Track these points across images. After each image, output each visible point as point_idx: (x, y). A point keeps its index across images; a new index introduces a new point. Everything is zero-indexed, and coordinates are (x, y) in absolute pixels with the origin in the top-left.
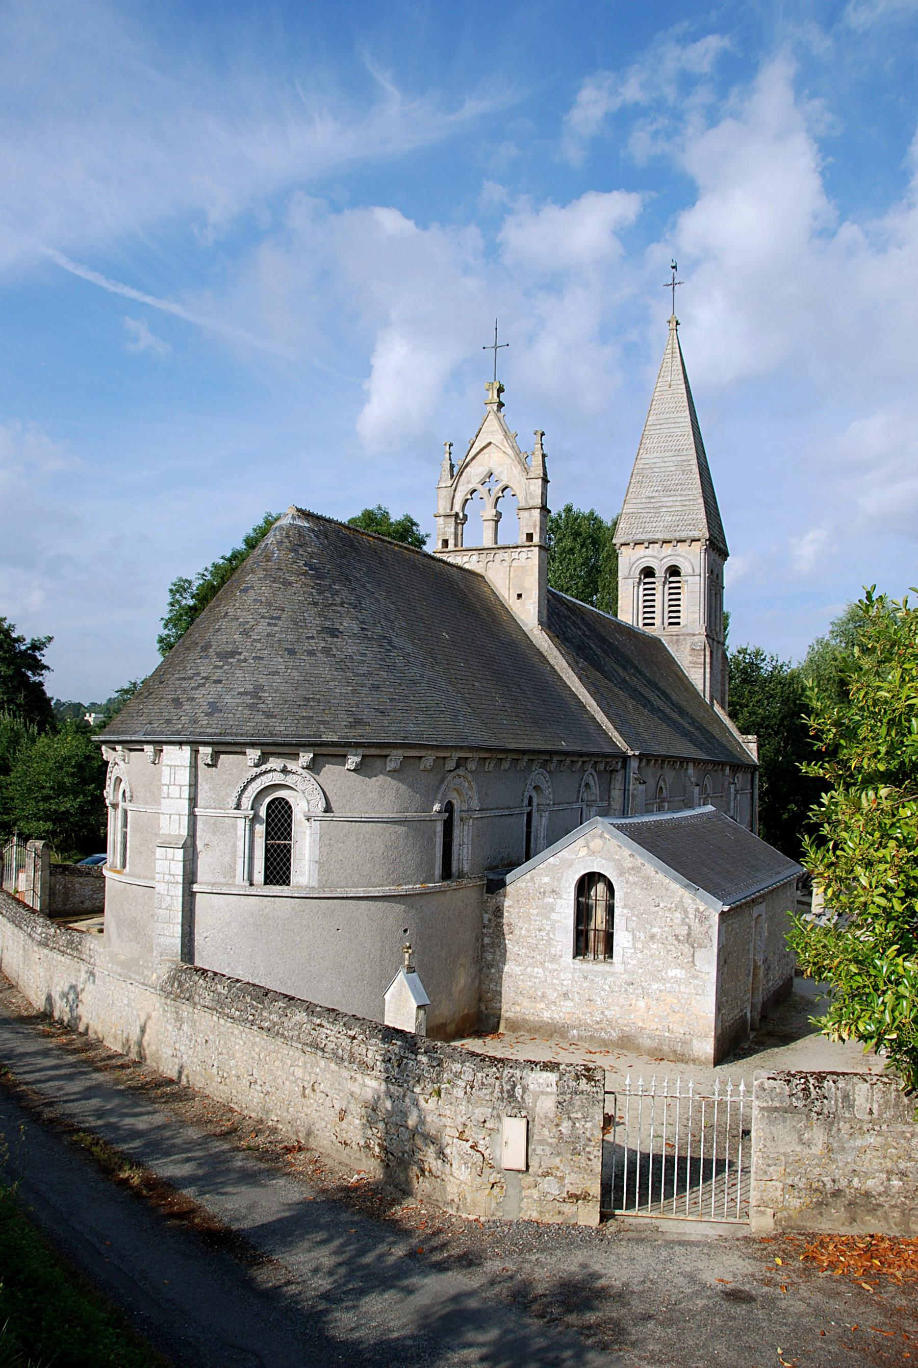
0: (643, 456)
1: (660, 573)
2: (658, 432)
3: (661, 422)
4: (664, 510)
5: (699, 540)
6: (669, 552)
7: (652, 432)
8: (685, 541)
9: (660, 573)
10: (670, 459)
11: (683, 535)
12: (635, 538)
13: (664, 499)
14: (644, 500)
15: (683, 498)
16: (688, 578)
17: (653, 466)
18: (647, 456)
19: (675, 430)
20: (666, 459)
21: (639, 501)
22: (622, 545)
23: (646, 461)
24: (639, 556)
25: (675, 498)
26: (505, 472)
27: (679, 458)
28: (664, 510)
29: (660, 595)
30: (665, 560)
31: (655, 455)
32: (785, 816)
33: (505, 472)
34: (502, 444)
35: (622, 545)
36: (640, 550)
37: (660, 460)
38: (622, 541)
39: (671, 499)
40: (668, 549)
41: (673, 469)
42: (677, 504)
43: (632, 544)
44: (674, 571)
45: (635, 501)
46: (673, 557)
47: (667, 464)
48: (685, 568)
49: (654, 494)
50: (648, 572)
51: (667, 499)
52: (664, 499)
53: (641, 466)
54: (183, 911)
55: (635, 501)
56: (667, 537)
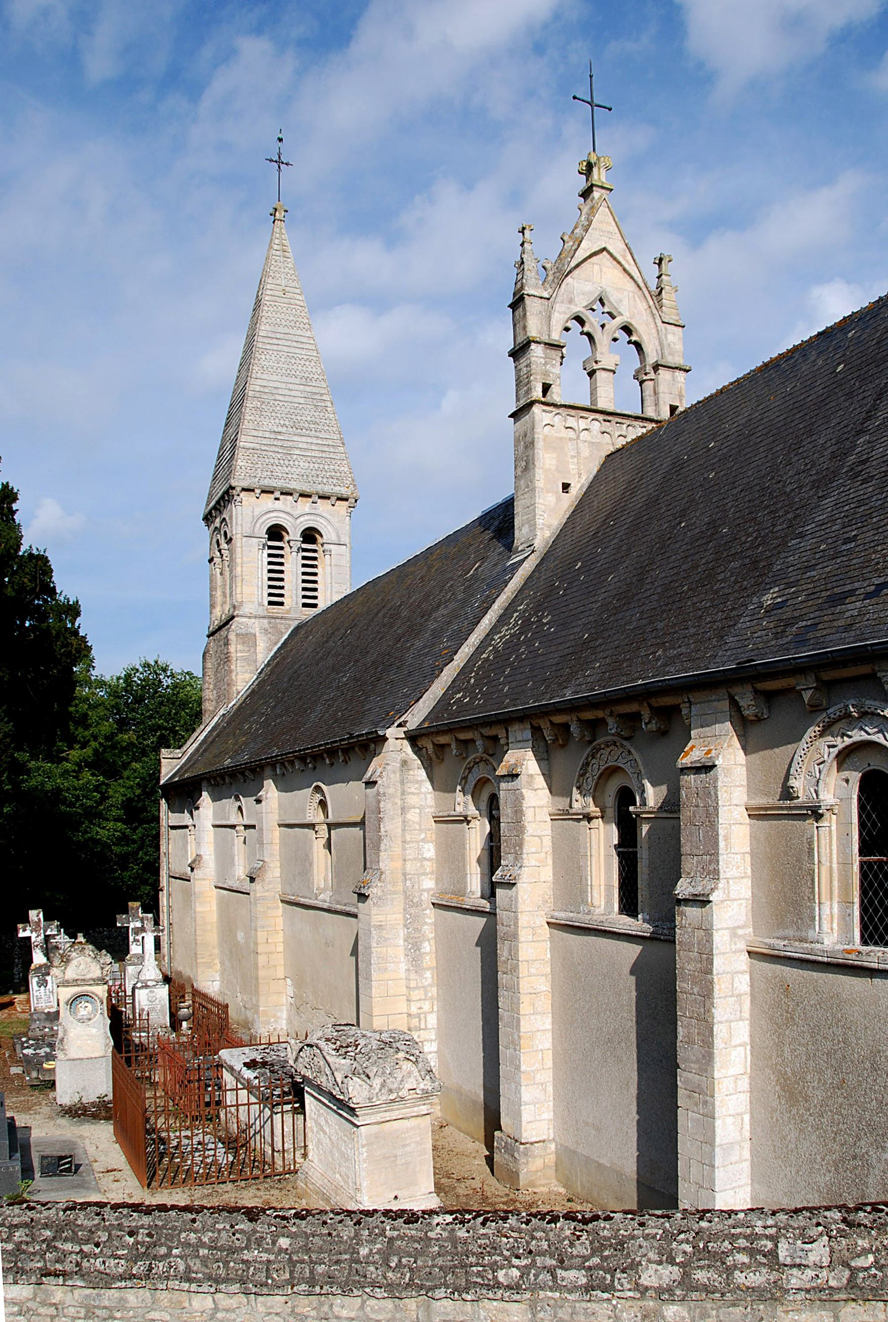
0: (259, 375)
1: (294, 534)
2: (275, 347)
3: (278, 336)
4: (297, 452)
5: (346, 500)
6: (307, 510)
7: (268, 347)
8: (328, 498)
9: (294, 534)
10: (297, 387)
11: (327, 489)
12: (262, 483)
13: (295, 438)
14: (267, 435)
15: (320, 442)
16: (331, 546)
17: (274, 391)
18: (264, 376)
19: (297, 351)
20: (290, 386)
21: (260, 434)
22: (244, 490)
23: (265, 383)
24: (265, 509)
25: (309, 440)
26: (625, 302)
27: (308, 389)
28: (297, 452)
29: (293, 565)
30: (302, 519)
31: (274, 378)
32: (48, 894)
33: (625, 302)
34: (624, 257)
35: (244, 490)
36: (267, 501)
37: (283, 386)
38: (245, 484)
39: (304, 439)
40: (305, 505)
41: (302, 401)
42: (313, 447)
43: (258, 491)
44: (310, 535)
45: (255, 433)
46: (312, 517)
47: (293, 393)
48: (328, 533)
49: (280, 429)
50: (276, 533)
51: (299, 439)
52: (295, 438)
53: (258, 388)
54: (638, 1061)
55: (255, 433)
56: (307, 489)
